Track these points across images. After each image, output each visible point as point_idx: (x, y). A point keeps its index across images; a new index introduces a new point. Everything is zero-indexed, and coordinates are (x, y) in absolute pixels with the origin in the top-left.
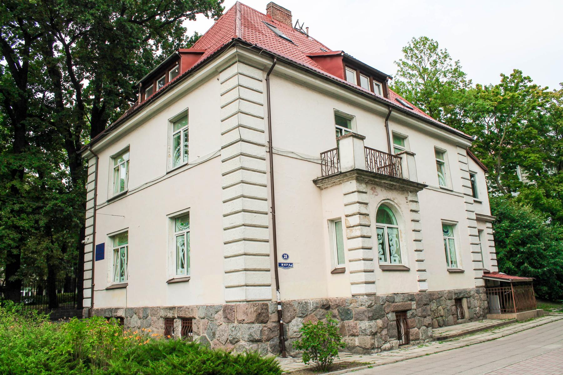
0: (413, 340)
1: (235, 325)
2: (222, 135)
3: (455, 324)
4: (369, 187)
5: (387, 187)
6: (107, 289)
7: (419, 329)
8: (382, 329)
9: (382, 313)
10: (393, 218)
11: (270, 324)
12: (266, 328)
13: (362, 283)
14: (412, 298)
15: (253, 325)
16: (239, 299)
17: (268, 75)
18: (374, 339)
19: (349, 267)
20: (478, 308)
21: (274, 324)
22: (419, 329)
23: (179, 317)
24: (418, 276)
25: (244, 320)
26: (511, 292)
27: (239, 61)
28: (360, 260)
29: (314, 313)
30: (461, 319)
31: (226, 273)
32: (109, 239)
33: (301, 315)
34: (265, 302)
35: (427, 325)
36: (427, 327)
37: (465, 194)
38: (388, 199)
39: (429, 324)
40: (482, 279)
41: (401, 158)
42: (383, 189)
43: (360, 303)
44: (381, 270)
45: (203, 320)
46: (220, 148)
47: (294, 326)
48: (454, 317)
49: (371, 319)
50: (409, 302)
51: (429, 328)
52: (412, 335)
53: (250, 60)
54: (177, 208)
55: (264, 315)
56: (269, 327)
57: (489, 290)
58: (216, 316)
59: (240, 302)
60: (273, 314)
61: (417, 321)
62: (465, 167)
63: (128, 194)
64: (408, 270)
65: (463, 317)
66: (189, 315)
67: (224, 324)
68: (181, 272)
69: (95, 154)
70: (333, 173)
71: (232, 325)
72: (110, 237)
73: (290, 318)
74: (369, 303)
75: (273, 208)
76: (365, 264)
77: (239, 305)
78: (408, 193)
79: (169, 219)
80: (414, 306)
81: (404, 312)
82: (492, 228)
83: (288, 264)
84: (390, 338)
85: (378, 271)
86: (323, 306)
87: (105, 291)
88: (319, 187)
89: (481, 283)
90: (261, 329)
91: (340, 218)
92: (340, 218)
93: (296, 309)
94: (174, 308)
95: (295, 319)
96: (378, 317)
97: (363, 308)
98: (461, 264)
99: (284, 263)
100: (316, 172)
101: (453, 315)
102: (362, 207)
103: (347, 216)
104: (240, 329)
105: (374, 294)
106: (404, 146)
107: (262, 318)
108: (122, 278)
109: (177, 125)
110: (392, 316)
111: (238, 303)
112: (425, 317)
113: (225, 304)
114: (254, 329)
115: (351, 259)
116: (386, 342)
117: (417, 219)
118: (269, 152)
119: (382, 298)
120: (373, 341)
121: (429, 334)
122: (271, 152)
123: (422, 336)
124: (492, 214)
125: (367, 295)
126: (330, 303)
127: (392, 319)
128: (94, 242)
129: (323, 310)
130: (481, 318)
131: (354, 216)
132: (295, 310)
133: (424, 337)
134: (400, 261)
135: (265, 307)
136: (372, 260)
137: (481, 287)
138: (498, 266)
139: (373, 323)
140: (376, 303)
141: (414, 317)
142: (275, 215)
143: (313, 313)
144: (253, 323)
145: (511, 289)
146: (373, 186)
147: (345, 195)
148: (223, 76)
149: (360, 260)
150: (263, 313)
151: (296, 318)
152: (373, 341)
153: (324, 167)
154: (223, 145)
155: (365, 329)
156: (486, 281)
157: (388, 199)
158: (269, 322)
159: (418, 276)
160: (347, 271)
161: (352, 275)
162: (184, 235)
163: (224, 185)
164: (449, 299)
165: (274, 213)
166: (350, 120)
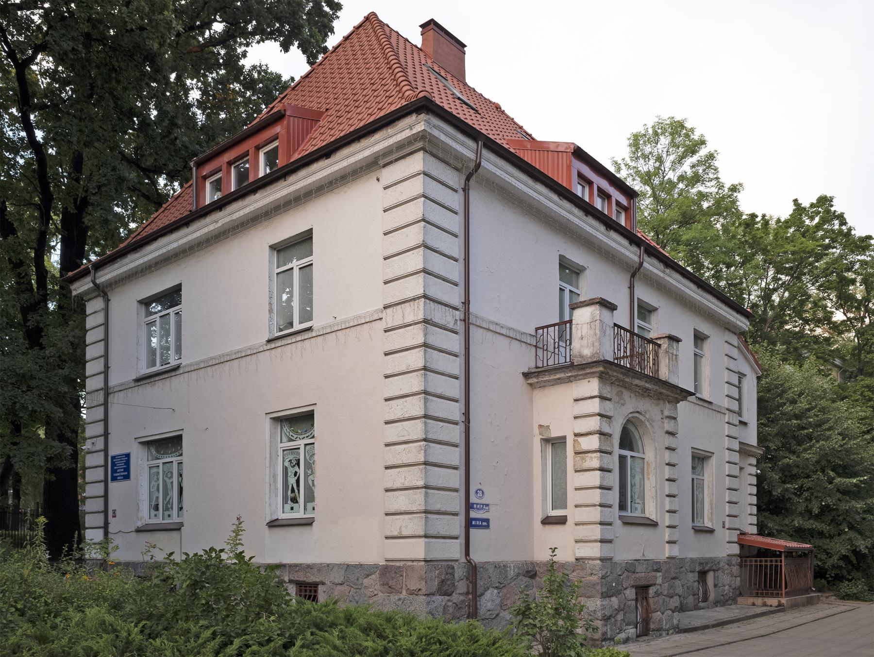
0: (654, 630)
1: (402, 596)
2: (385, 283)
3: (695, 609)
4: (615, 390)
5: (639, 393)
6: (139, 531)
7: (663, 614)
8: (618, 611)
9: (619, 588)
10: (639, 442)
11: (456, 598)
12: (450, 604)
13: (596, 541)
14: (656, 566)
15: (434, 598)
16: (413, 557)
17: (468, 179)
18: (606, 625)
19: (572, 513)
20: (727, 587)
21: (462, 598)
22: (663, 614)
23: (291, 581)
24: (667, 534)
25: (420, 589)
26: (781, 566)
27: (423, 149)
28: (595, 505)
29: (515, 582)
30: (703, 602)
31: (387, 514)
32: (140, 447)
33: (497, 585)
34: (450, 563)
35: (673, 608)
36: (673, 612)
37: (728, 409)
38: (638, 412)
39: (676, 607)
40: (736, 545)
41: (659, 346)
42: (632, 395)
43: (589, 571)
44: (621, 523)
45: (339, 587)
46: (382, 307)
47: (488, 601)
48: (695, 599)
49: (605, 595)
50: (654, 573)
51: (675, 614)
52: (654, 623)
53: (446, 148)
54: (293, 404)
55: (449, 582)
56: (454, 601)
57: (746, 561)
58: (366, 581)
59: (413, 561)
60: (461, 582)
61: (661, 602)
62: (733, 365)
63: (181, 371)
64: (654, 525)
65: (705, 599)
66: (312, 579)
67: (380, 594)
68: (292, 508)
69: (102, 291)
70: (556, 362)
71: (397, 597)
72: (140, 443)
73: (482, 588)
74: (604, 572)
75: (467, 414)
76: (601, 512)
77: (412, 567)
78: (664, 403)
79: (272, 421)
80: (659, 581)
81: (647, 587)
82: (756, 466)
83: (483, 505)
84: (627, 625)
85: (618, 523)
86: (528, 572)
87: (134, 534)
88: (531, 385)
89: (735, 549)
90: (444, 603)
91: (564, 438)
92: (564, 438)
93: (491, 575)
94: (284, 566)
95: (489, 591)
96: (613, 593)
97: (594, 578)
98: (711, 520)
99: (477, 504)
100: (527, 360)
101: (694, 595)
102: (604, 423)
103: (576, 435)
104: (411, 603)
105: (611, 559)
106: (650, 324)
107: (445, 588)
108: (167, 513)
109: (282, 254)
110: (630, 593)
111: (410, 563)
112: (672, 597)
113: (383, 563)
114: (436, 604)
115: (579, 503)
116: (621, 630)
117: (673, 446)
118: (464, 320)
119: (621, 564)
120: (605, 629)
121: (675, 622)
122: (466, 320)
123: (666, 625)
124: (758, 445)
125: (426, 561)
126: (537, 569)
127: (630, 597)
128: (106, 450)
129: (527, 579)
130: (730, 602)
131: (590, 436)
132: (490, 578)
133: (668, 626)
134: (643, 511)
135: (450, 571)
136: (610, 507)
137: (734, 555)
138: (757, 525)
139: (606, 602)
140: (611, 573)
141: (659, 595)
142: (469, 427)
143: (513, 583)
144: (434, 595)
145: (781, 561)
146: (620, 389)
147: (576, 400)
148: (390, 174)
149: (595, 505)
150: (448, 580)
151: (491, 590)
152: (605, 629)
153: (540, 352)
154: (389, 301)
155: (595, 611)
156: (742, 546)
157: (638, 412)
158: (454, 594)
159: (667, 534)
160: (570, 522)
161: (578, 527)
162: (299, 448)
163: (389, 372)
164: (691, 572)
165: (469, 423)
166: (578, 274)
